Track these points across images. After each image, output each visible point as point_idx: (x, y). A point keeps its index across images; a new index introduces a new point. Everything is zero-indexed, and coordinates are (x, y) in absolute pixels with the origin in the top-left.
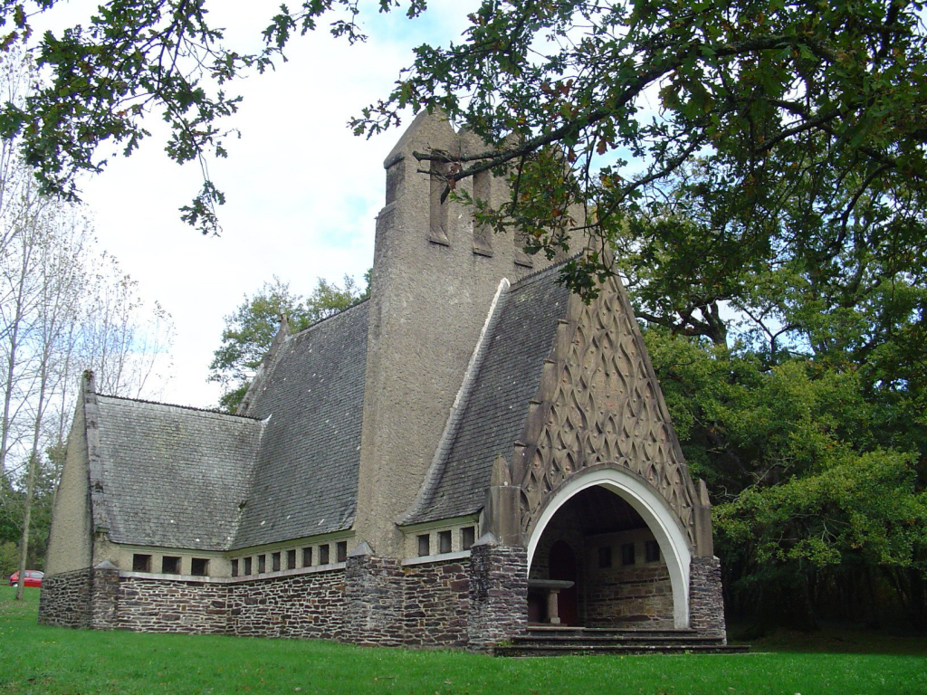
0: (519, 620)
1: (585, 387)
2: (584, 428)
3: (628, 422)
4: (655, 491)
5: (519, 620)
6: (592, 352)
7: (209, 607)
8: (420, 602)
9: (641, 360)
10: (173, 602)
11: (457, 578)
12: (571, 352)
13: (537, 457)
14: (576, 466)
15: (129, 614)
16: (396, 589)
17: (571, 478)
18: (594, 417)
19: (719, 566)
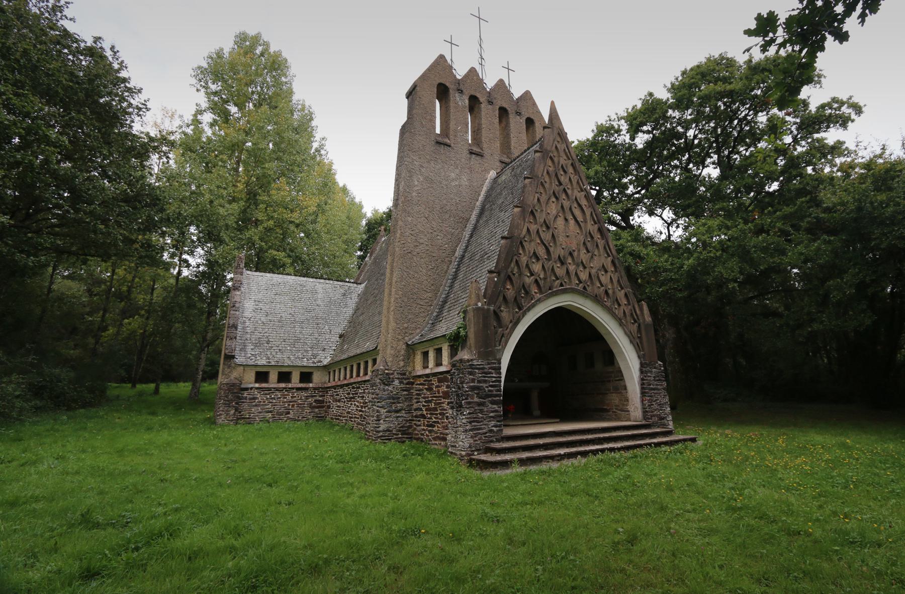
0: (493, 428)
1: (548, 228)
2: (549, 259)
3: (584, 256)
4: (610, 311)
5: (493, 428)
6: (553, 202)
7: (312, 404)
8: (424, 406)
9: (592, 210)
10: (285, 402)
11: (446, 388)
12: (536, 200)
13: (508, 283)
14: (543, 289)
15: (250, 413)
16: (407, 395)
17: (539, 301)
18: (556, 252)
19: (662, 368)
